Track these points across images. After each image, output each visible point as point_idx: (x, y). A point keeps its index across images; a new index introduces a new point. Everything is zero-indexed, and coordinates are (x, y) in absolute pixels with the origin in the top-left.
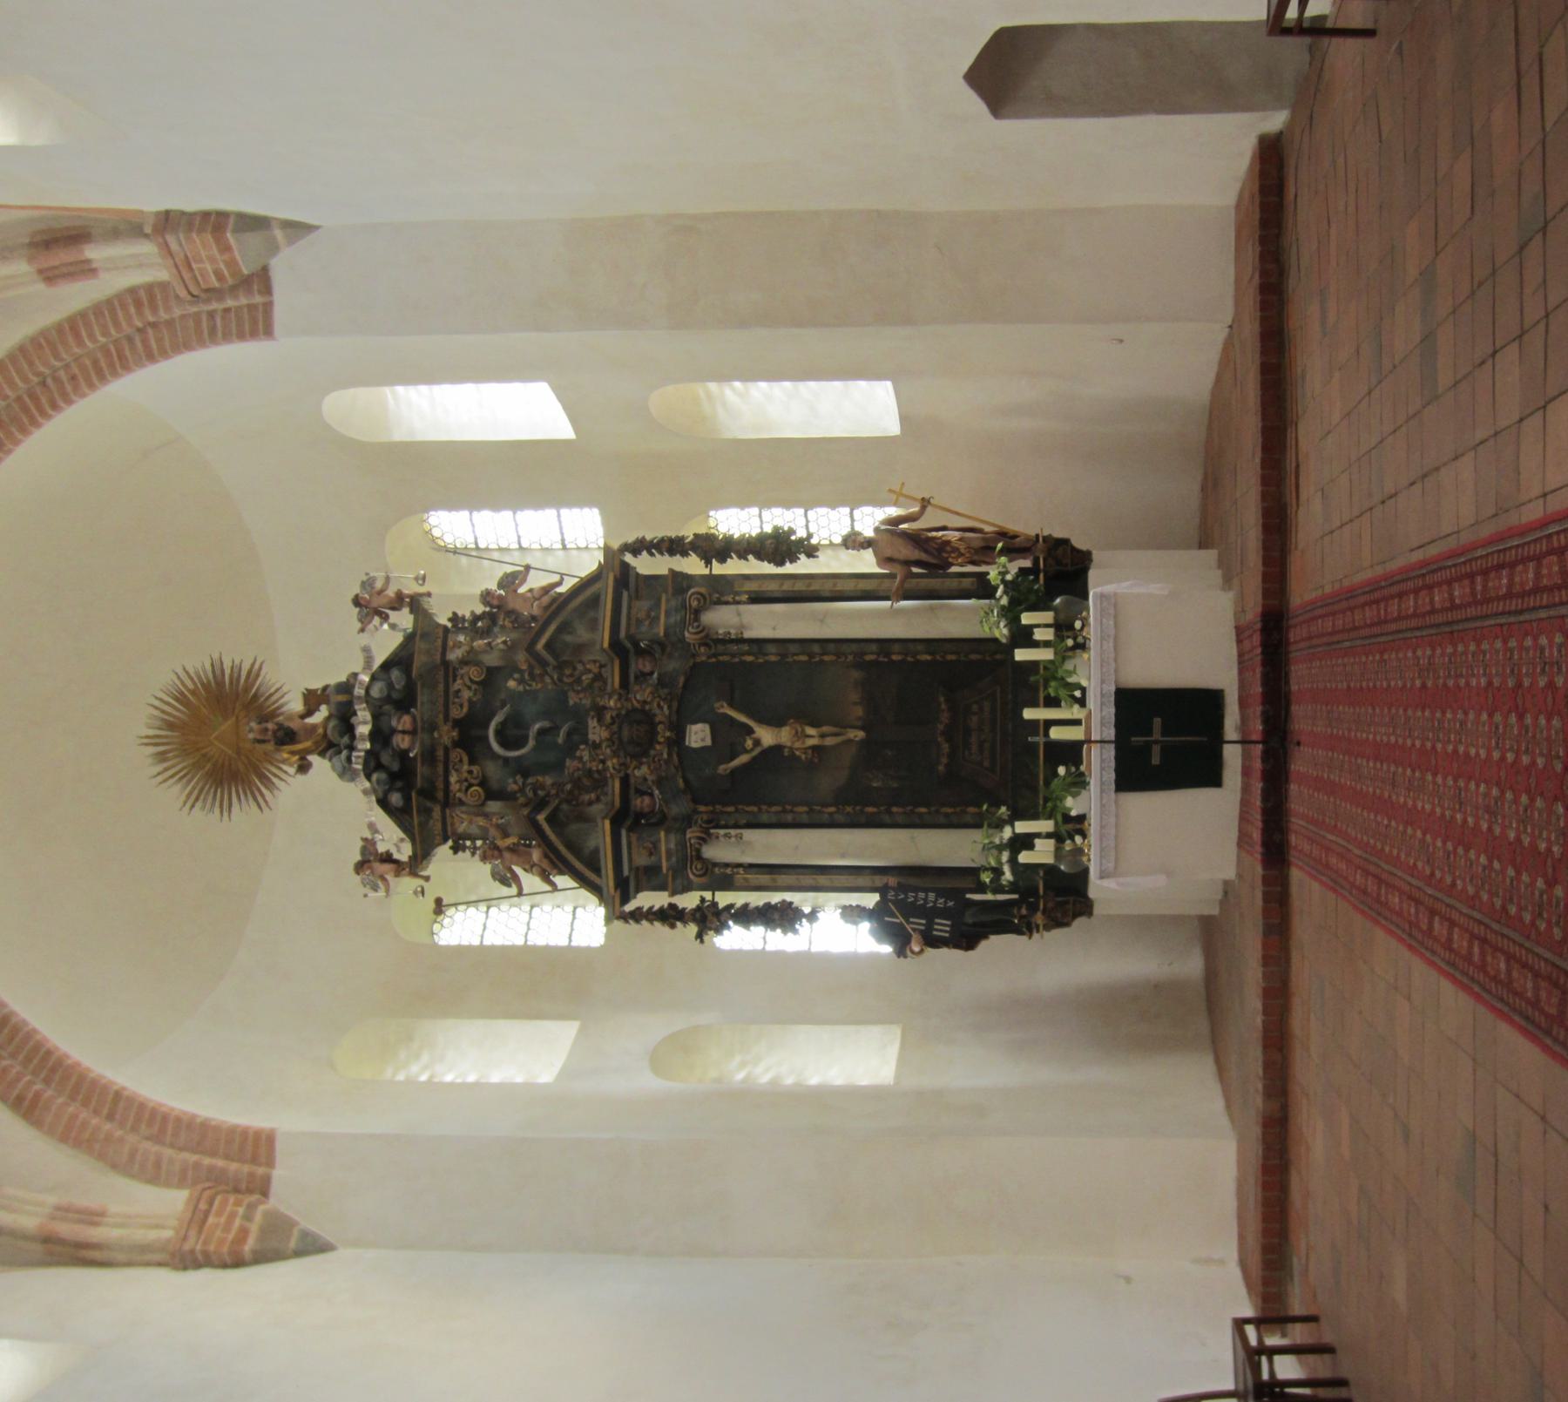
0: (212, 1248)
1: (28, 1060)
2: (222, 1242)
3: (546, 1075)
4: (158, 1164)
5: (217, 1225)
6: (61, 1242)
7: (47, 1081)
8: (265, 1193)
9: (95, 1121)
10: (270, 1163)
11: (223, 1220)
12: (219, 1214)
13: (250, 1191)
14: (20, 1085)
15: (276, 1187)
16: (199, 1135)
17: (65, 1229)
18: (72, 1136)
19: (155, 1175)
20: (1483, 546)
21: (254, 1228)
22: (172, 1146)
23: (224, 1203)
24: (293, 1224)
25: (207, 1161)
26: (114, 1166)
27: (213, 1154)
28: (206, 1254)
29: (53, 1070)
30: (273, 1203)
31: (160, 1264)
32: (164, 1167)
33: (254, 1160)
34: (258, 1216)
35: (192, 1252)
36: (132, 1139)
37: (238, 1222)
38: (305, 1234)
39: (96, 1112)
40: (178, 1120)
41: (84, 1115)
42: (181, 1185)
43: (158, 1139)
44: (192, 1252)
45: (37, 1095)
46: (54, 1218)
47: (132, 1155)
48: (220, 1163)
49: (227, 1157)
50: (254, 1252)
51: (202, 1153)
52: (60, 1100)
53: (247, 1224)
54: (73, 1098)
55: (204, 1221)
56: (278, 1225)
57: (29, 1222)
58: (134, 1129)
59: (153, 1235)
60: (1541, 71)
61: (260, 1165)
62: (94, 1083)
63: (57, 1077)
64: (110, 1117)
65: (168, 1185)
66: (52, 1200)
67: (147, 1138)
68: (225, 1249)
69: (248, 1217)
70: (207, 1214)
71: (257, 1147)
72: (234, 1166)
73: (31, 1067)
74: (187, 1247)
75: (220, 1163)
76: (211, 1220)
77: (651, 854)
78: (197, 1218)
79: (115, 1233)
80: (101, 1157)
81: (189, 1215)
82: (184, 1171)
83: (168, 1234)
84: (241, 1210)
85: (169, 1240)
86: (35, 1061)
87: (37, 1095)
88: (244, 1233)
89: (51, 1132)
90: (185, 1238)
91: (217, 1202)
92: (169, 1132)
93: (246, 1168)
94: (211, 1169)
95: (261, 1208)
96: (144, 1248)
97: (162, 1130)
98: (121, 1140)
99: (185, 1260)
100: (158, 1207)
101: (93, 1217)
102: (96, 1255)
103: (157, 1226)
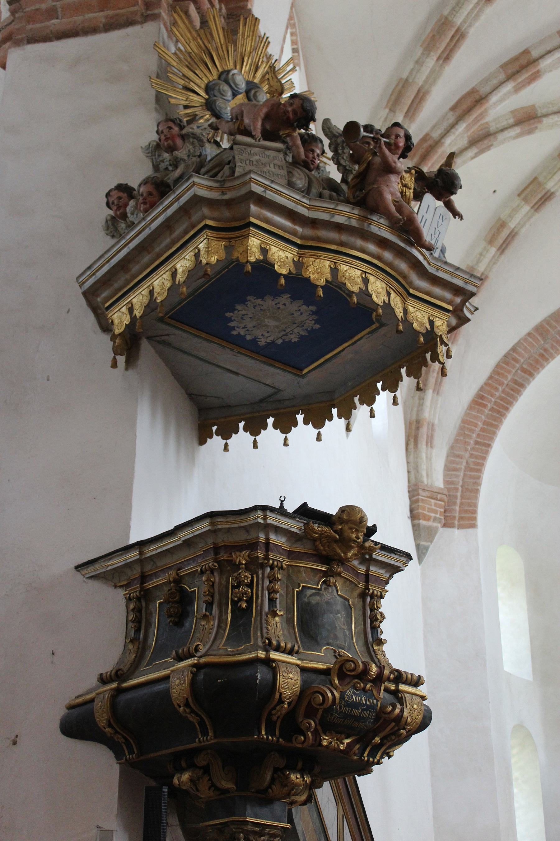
0: (420, 504)
1: (502, 399)
2: (424, 509)
3: (507, 667)
4: (455, 470)
5: (431, 505)
6: (418, 428)
7: (492, 409)
8: (445, 526)
9: (474, 436)
10: (460, 527)
11: (433, 507)
12: (436, 505)
13: (445, 517)
14: (489, 397)
15: (448, 531)
16: (471, 490)
17: (424, 430)
18: (466, 425)
19: (449, 469)
20: (509, 242)
21: (430, 523)
22: (465, 475)
23: (440, 506)
24: (431, 542)
25: (459, 494)
26: (452, 448)
27: (462, 497)
28: (417, 501)
29: (499, 412)
30: (441, 530)
31: (153, 163)
32: (454, 473)
33: (461, 518)
34: (435, 524)
35: (418, 495)
36: (467, 455)
37: (433, 515)
38: (427, 548)
39: (478, 435)
40: (479, 478)
41: (477, 430)
42: (446, 482)
43: (468, 468)
44: (418, 495)
45: (485, 406)
46: (428, 424)
47: (458, 456)
48: (458, 501)
49: (462, 504)
50: (419, 525)
51: (462, 491)
52: (483, 417)
53: (432, 520)
54: (484, 423)
55: (432, 498)
56: (431, 534)
57: (426, 414)
58: (471, 455)
59: (424, 473)
60: (181, 351)
61: (459, 522)
62: (494, 433)
63: (495, 414)
64: (477, 443)
65: (445, 475)
66: (436, 422)
67: (467, 463)
68: (420, 511)
69: (435, 519)
70: (436, 499)
71: (468, 520)
72: (457, 508)
73: (499, 401)
74: (421, 492)
75: (458, 501)
76: (433, 501)
77: (265, 166)
78: (434, 495)
79: (424, 455)
80: (456, 441)
81: (435, 490)
82: (452, 483)
83: (425, 480)
84: (438, 516)
85: (422, 482)
86: (502, 402)
87: (485, 406)
88: (428, 519)
89: (466, 414)
90: (424, 490)
91: (440, 502)
92: (473, 474)
93: (457, 515)
94: (456, 497)
95: (439, 525)
96: (417, 469)
97: (472, 470)
98: (466, 450)
99: (414, 491)
100: (436, 476)
101: (430, 442)
102: (412, 446)
103: (427, 475)
